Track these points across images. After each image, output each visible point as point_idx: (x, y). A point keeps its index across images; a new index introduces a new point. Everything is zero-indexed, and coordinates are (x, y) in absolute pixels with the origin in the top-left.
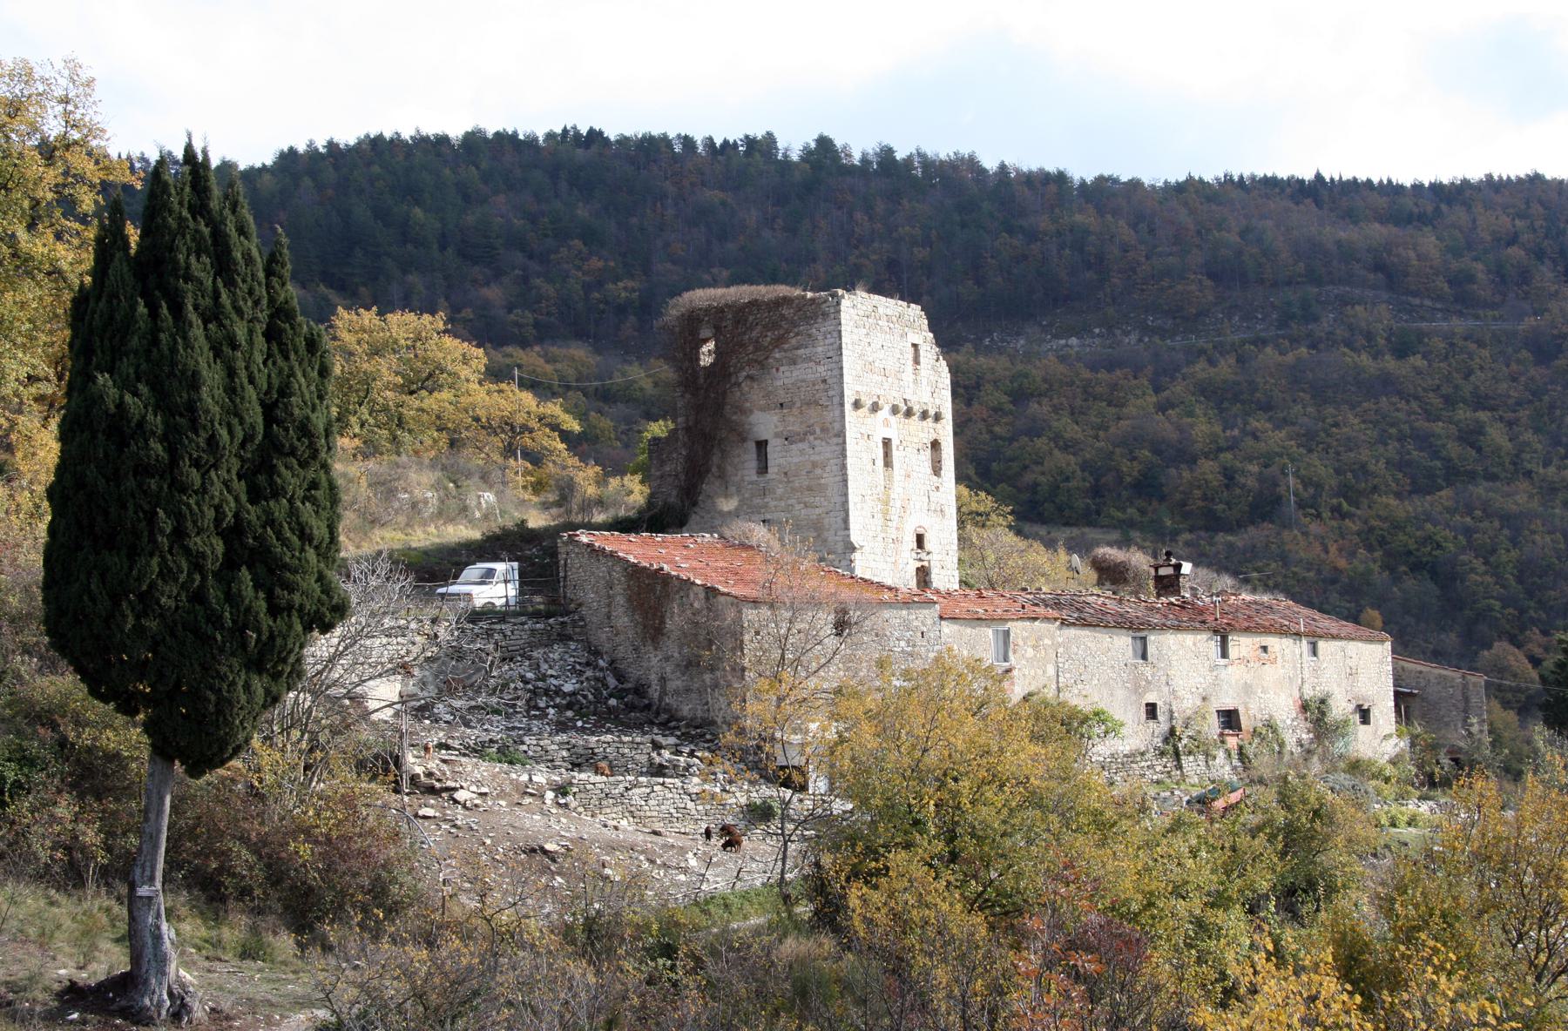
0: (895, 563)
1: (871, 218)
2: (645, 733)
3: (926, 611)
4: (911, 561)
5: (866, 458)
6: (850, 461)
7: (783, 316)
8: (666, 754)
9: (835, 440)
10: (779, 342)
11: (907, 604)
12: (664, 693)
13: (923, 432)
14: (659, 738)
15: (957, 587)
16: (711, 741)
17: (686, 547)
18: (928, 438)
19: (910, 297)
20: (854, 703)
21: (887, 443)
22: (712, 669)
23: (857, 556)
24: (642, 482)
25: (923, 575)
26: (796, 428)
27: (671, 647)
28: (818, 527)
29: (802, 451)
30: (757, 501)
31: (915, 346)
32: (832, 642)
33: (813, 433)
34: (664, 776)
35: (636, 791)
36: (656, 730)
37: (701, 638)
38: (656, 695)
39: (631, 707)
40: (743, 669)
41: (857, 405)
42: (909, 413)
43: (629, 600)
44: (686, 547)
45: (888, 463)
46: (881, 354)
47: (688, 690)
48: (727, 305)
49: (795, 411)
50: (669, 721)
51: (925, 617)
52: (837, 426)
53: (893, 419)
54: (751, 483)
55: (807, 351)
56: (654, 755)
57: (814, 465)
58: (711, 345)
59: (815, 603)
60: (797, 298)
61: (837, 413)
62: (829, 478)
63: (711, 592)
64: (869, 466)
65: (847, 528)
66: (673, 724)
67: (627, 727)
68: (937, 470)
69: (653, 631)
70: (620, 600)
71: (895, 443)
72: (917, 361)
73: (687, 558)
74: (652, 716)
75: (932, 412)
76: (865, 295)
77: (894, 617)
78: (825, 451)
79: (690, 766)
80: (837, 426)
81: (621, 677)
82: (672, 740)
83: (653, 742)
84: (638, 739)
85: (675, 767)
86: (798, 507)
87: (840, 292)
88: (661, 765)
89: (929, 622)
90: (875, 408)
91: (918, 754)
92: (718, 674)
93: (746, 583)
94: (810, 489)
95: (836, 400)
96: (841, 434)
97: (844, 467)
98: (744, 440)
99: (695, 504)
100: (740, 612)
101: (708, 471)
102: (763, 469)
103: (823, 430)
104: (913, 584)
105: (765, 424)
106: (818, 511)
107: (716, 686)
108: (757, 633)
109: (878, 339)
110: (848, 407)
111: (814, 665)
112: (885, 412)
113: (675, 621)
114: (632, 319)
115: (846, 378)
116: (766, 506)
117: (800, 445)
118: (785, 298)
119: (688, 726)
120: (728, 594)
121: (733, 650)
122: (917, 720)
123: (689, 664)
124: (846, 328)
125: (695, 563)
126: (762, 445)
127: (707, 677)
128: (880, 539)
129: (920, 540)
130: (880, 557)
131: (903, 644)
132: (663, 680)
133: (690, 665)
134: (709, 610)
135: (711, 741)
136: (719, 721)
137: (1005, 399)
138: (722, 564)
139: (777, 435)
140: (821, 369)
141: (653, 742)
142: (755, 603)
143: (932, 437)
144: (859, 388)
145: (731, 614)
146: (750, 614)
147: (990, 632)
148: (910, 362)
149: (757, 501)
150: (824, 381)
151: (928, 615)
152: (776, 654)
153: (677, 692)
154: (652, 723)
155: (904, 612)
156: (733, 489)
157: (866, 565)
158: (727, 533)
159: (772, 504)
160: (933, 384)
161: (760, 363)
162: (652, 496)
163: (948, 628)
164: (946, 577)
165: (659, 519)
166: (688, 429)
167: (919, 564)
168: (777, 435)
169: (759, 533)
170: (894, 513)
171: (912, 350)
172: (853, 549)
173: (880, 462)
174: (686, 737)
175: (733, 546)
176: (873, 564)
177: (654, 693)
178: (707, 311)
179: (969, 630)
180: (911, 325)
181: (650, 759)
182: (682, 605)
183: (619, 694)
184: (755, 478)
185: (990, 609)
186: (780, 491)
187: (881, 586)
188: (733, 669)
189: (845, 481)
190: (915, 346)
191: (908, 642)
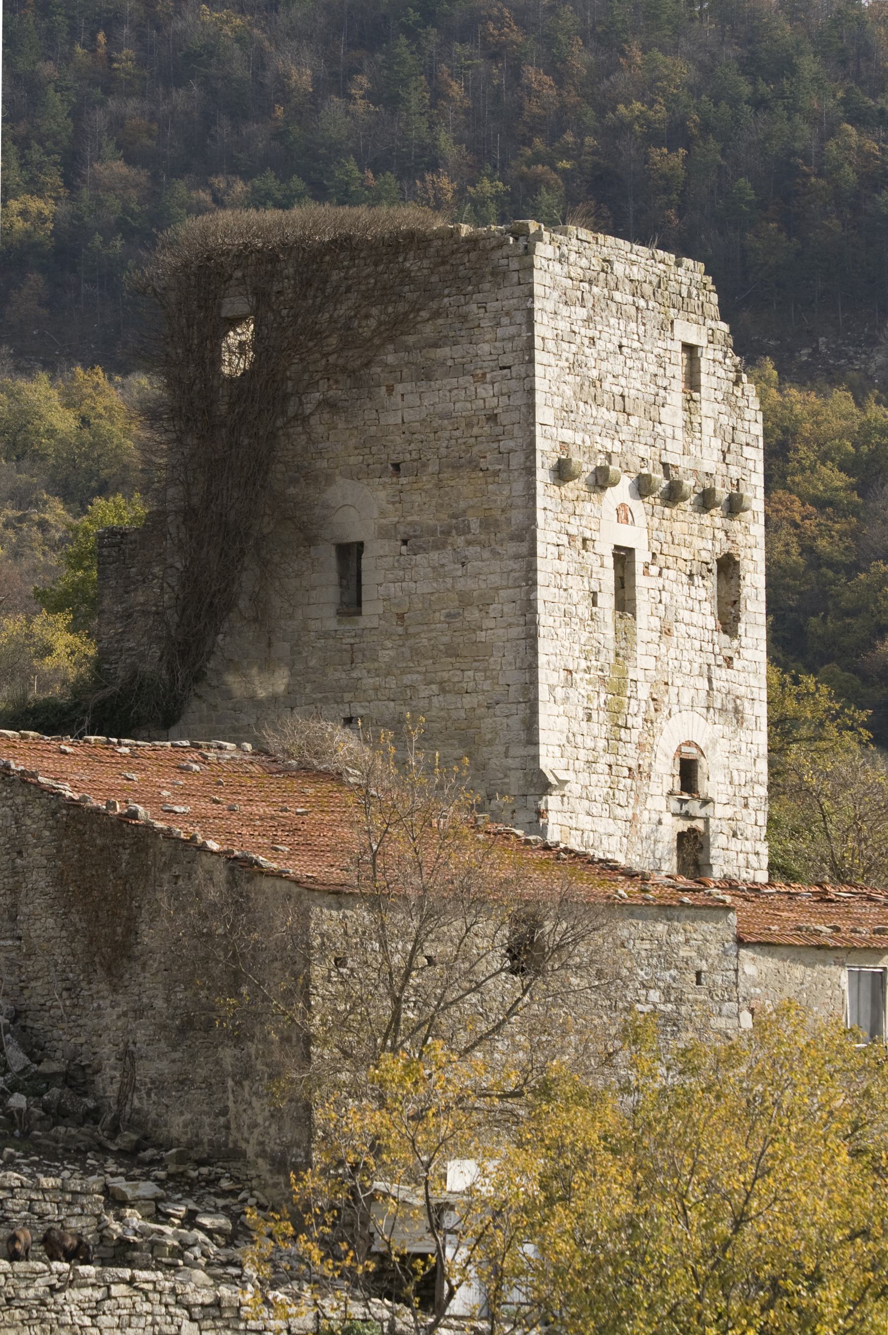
0: (632, 821)
1: (560, 82)
2: (88, 1172)
3: (705, 926)
4: (667, 818)
5: (578, 588)
6: (542, 594)
7: (405, 276)
8: (135, 1218)
9: (512, 548)
10: (395, 329)
11: (667, 910)
12: (129, 1086)
13: (699, 536)
14: (119, 1183)
15: (762, 877)
16: (233, 1193)
17: (184, 770)
18: (709, 549)
19: (683, 248)
20: (580, 1116)
21: (623, 558)
22: (238, 1038)
23: (552, 801)
24: (72, 629)
25: (693, 847)
26: (428, 519)
27: (148, 984)
28: (466, 736)
29: (438, 570)
30: (337, 675)
31: (690, 349)
32: (504, 987)
33: (466, 530)
34: (130, 1264)
35: (74, 1294)
36: (112, 1167)
37: (217, 970)
38: (112, 1091)
39: (57, 1114)
40: (308, 1040)
41: (563, 472)
42: (673, 495)
43: (59, 881)
44: (184, 770)
45: (625, 602)
46: (616, 365)
47: (183, 1082)
48: (285, 247)
49: (426, 481)
50: (139, 1147)
51: (703, 940)
52: (517, 516)
53: (638, 507)
54: (324, 635)
55: (458, 352)
56: (109, 1219)
57: (465, 600)
58: (244, 333)
59: (472, 900)
60: (438, 235)
61: (519, 487)
62: (496, 631)
63: (242, 868)
64: (584, 610)
65: (532, 740)
66: (150, 1153)
67: (50, 1156)
68: (728, 620)
69: (111, 952)
70: (39, 880)
71: (641, 557)
72: (692, 382)
73: (186, 794)
74: (102, 1135)
75: (722, 494)
76: (585, 234)
77: (640, 936)
78: (491, 572)
79: (186, 1246)
80: (517, 516)
81: (36, 1050)
82: (147, 1189)
83: (106, 1191)
84: (75, 1185)
85: (155, 1246)
86: (424, 692)
87: (533, 226)
88: (123, 1242)
89: (714, 950)
90: (601, 480)
91: (724, 1228)
92: (252, 1048)
93: (317, 853)
94: (452, 651)
95: (517, 460)
96: (527, 534)
97: (529, 607)
98: (311, 541)
99: (199, 677)
100: (305, 915)
101: (230, 606)
102: (352, 603)
103: (487, 524)
104: (670, 866)
105: (360, 508)
106: (468, 701)
107: (245, 1073)
108: (340, 962)
109: (612, 331)
110: (543, 476)
111: (463, 1038)
112: (621, 492)
113: (158, 932)
114: (35, 279)
115: (543, 414)
116: (355, 687)
117: (434, 555)
118: (411, 235)
119: (181, 1158)
120: (279, 875)
121: (288, 996)
122: (727, 1152)
123: (187, 1026)
124: (545, 303)
125: (204, 806)
126: (350, 554)
127: (227, 1055)
128: (602, 767)
129: (688, 772)
130: (599, 808)
131: (655, 996)
132: (128, 1057)
133: (191, 1028)
134: (239, 908)
135: (233, 1193)
136: (251, 1150)
137: (840, 479)
138: (261, 809)
139: (384, 533)
140: (486, 391)
141: (106, 1191)
142: (339, 895)
143: (722, 547)
144: (567, 435)
145: (284, 922)
146: (326, 920)
147: (844, 977)
148: (678, 385)
149: (337, 675)
150: (493, 418)
151: (707, 937)
152: (383, 1009)
153: (158, 1085)
154: (102, 1150)
155: (661, 928)
156: (282, 648)
157: (569, 822)
158: (273, 743)
159: (369, 682)
160: (721, 431)
161: (352, 374)
162: (103, 656)
163: (753, 966)
164: (742, 853)
165: (114, 708)
166: (189, 514)
167: (683, 826)
168: (384, 533)
169: (345, 744)
170: (636, 709)
171: (680, 357)
172: (544, 787)
173: (607, 601)
174: (179, 1184)
175: (286, 770)
176: (585, 822)
177: (108, 1084)
178: (243, 255)
179: (799, 971)
180: (682, 304)
181: (101, 1230)
182: (175, 895)
183: (31, 1083)
184: (332, 624)
185: (845, 926)
186: (386, 656)
187: (609, 867)
188: (286, 1039)
189: (531, 638)
190: (690, 349)
191: (666, 992)
